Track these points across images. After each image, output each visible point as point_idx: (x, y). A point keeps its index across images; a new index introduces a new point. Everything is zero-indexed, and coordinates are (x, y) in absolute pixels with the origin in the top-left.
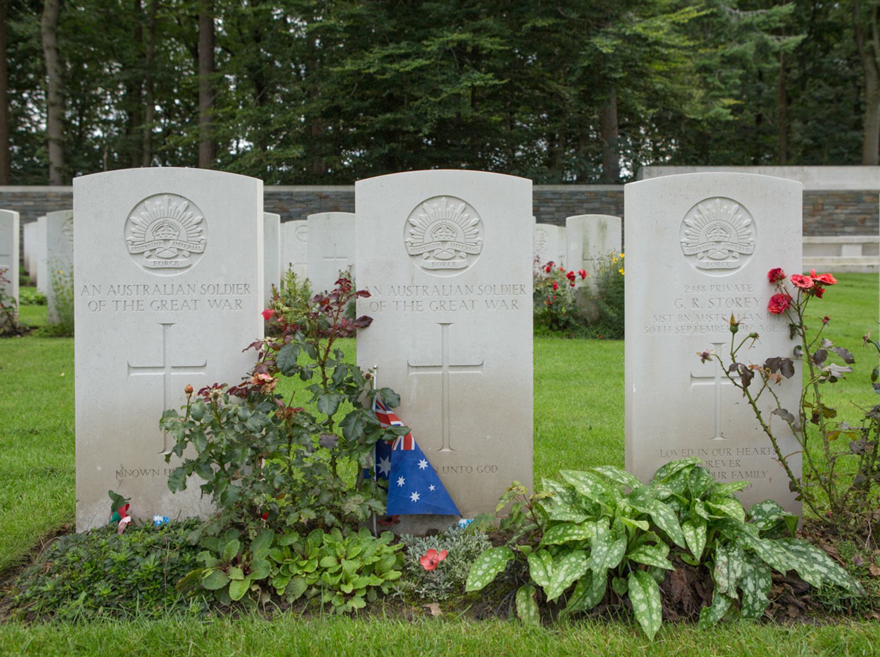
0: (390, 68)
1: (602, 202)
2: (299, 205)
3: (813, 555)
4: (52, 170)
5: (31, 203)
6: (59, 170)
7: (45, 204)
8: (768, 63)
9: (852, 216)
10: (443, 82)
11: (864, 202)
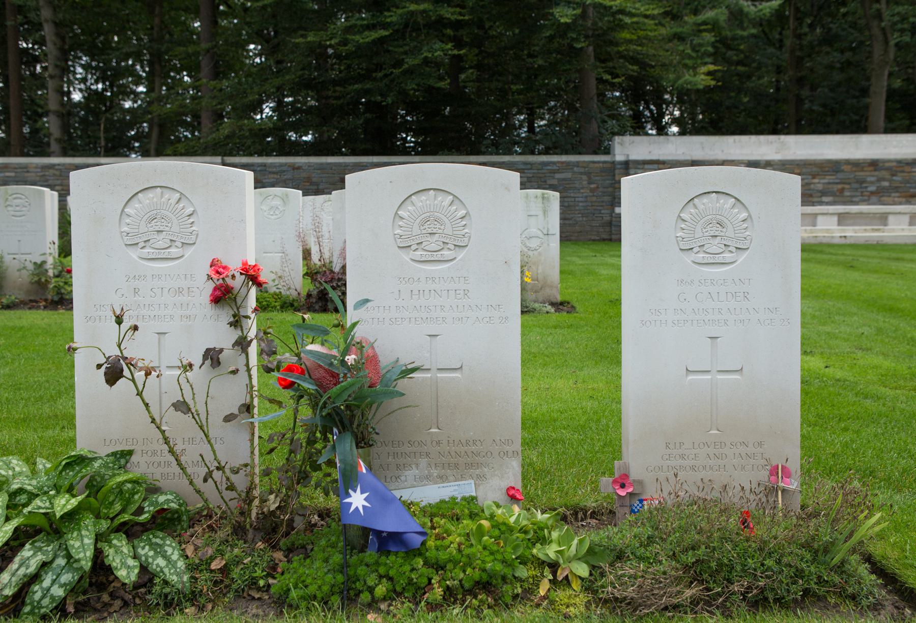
0: (353, 40)
1: (574, 173)
2: (272, 176)
3: (166, 548)
4: (53, 143)
5: (13, 174)
6: (59, 141)
7: (26, 174)
8: (743, 29)
9: (830, 186)
10: (406, 53)
11: (843, 171)
